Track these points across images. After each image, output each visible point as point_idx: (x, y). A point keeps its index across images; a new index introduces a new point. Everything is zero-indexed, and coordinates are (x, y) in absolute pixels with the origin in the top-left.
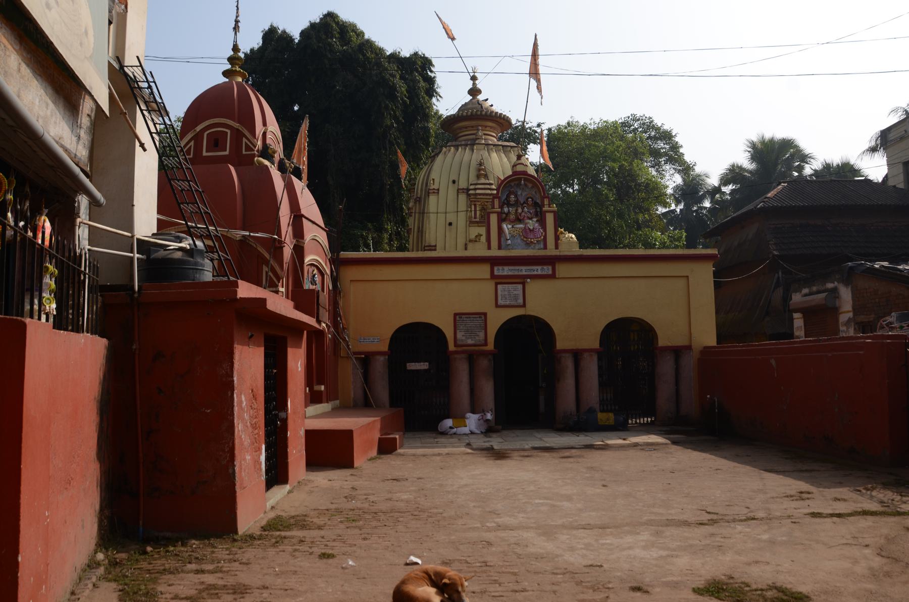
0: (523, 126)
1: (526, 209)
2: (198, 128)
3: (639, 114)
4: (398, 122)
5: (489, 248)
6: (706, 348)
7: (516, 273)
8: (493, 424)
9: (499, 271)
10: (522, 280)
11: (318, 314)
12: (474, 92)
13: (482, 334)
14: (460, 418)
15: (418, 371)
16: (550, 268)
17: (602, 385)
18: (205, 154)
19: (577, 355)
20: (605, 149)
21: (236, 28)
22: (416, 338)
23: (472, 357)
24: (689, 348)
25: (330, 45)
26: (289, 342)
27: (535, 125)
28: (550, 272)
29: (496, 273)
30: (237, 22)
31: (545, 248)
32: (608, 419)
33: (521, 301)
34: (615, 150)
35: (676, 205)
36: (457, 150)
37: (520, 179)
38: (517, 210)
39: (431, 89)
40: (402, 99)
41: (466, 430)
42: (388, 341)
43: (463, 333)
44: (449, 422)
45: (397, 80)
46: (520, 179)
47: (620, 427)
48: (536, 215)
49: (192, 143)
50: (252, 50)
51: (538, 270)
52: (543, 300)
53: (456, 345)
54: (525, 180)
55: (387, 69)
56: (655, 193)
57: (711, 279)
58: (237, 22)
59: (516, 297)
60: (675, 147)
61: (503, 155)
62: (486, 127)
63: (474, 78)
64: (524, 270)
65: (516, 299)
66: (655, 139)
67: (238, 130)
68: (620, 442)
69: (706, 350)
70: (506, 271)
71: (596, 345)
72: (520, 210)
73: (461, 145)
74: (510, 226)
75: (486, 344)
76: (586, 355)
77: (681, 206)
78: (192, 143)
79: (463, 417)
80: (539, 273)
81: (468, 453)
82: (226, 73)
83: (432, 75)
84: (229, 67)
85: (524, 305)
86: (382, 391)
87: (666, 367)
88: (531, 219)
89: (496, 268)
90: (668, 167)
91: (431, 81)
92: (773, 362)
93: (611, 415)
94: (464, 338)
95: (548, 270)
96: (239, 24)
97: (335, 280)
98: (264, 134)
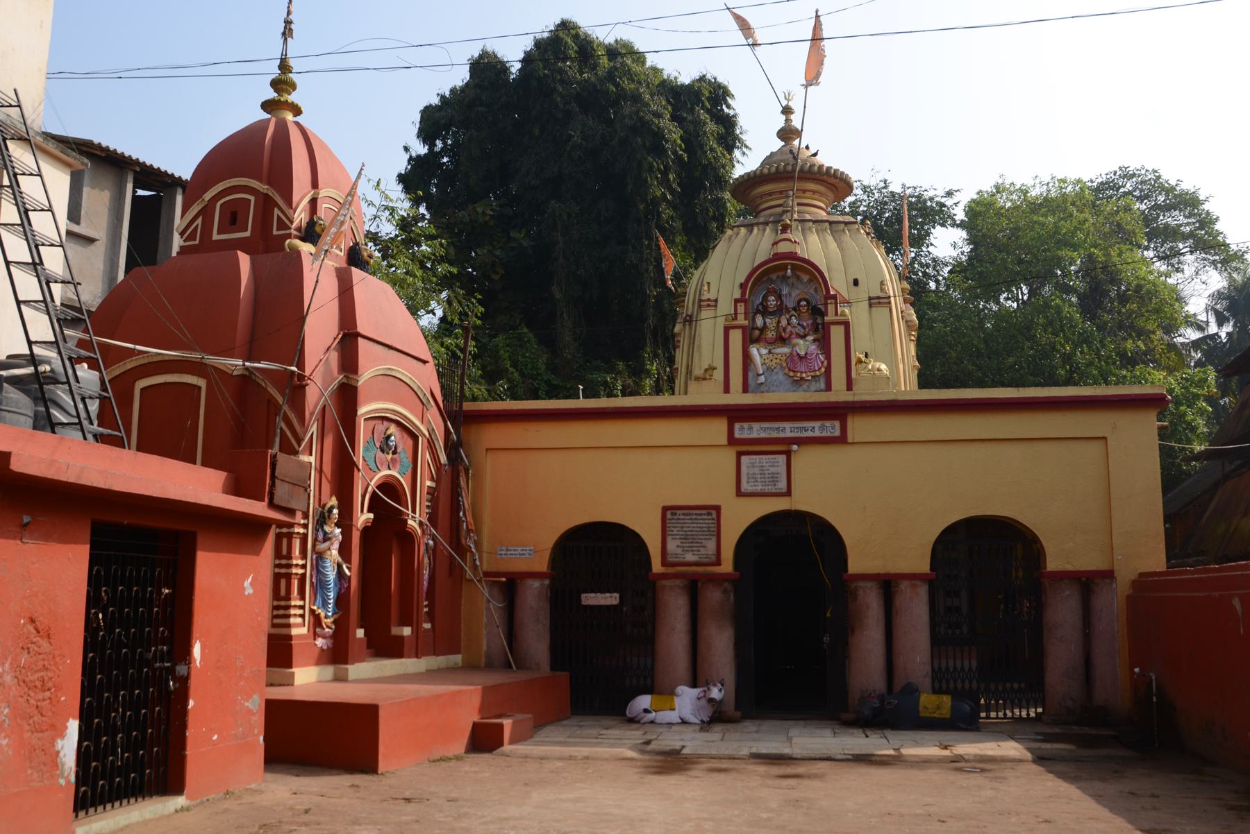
0: (443, 97)
1: (794, 320)
2: (208, 196)
3: (1133, 165)
4: (672, 192)
5: (727, 390)
6: (1142, 575)
7: (775, 435)
8: (730, 708)
9: (745, 431)
10: (785, 447)
11: (271, 495)
12: (788, 134)
13: (711, 545)
14: (662, 691)
15: (600, 608)
16: (837, 424)
17: (937, 641)
18: (216, 237)
19: (888, 584)
20: (1057, 230)
21: (287, 32)
22: (598, 549)
23: (694, 586)
24: (1109, 575)
25: (561, 71)
26: (200, 540)
27: (941, 192)
28: (837, 433)
29: (737, 434)
30: (288, 23)
31: (828, 387)
32: (939, 708)
33: (782, 485)
34: (1076, 228)
35: (1220, 324)
36: (751, 232)
37: (785, 267)
38: (779, 322)
39: (729, 135)
40: (675, 153)
41: (672, 716)
42: (547, 554)
43: (678, 542)
44: (644, 701)
45: (666, 123)
46: (785, 267)
47: (964, 721)
48: (816, 330)
49: (199, 221)
50: (453, 91)
51: (815, 428)
52: (822, 483)
53: (664, 563)
54: (794, 268)
55: (647, 105)
56: (1163, 307)
57: (1156, 442)
58: (288, 23)
59: (774, 479)
60: (1207, 222)
61: (830, 238)
62: (804, 191)
63: (787, 111)
64: (788, 429)
65: (774, 479)
66: (1168, 208)
67: (267, 195)
68: (933, 751)
69: (1144, 583)
70: (756, 430)
71: (924, 567)
72: (784, 322)
73: (757, 224)
74: (764, 351)
75: (718, 562)
76: (904, 585)
77: (1228, 328)
78: (199, 221)
79: (672, 693)
80: (817, 433)
81: (632, 759)
82: (267, 106)
83: (732, 113)
84: (271, 94)
85: (788, 493)
86: (537, 643)
87: (1063, 611)
88: (803, 337)
89: (737, 426)
90: (1189, 258)
91: (728, 123)
92: (1236, 603)
93: (946, 700)
94: (679, 551)
95: (833, 429)
96: (293, 26)
97: (453, 448)
98: (314, 202)
